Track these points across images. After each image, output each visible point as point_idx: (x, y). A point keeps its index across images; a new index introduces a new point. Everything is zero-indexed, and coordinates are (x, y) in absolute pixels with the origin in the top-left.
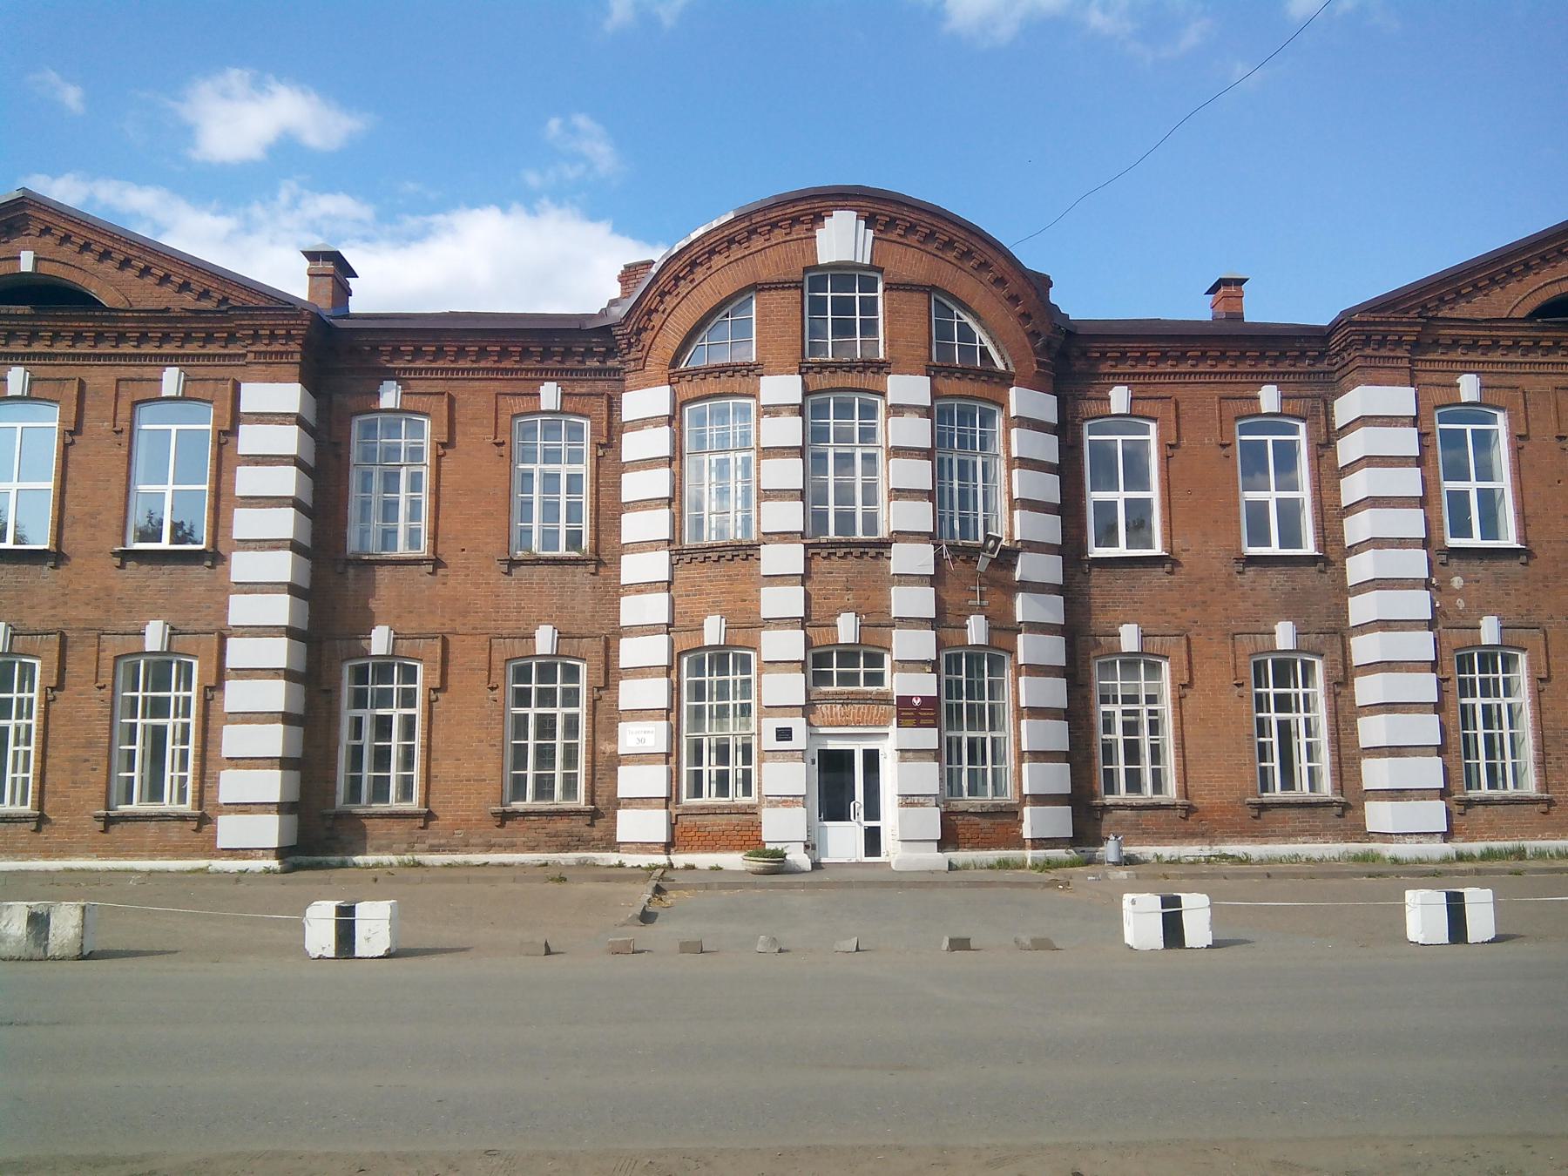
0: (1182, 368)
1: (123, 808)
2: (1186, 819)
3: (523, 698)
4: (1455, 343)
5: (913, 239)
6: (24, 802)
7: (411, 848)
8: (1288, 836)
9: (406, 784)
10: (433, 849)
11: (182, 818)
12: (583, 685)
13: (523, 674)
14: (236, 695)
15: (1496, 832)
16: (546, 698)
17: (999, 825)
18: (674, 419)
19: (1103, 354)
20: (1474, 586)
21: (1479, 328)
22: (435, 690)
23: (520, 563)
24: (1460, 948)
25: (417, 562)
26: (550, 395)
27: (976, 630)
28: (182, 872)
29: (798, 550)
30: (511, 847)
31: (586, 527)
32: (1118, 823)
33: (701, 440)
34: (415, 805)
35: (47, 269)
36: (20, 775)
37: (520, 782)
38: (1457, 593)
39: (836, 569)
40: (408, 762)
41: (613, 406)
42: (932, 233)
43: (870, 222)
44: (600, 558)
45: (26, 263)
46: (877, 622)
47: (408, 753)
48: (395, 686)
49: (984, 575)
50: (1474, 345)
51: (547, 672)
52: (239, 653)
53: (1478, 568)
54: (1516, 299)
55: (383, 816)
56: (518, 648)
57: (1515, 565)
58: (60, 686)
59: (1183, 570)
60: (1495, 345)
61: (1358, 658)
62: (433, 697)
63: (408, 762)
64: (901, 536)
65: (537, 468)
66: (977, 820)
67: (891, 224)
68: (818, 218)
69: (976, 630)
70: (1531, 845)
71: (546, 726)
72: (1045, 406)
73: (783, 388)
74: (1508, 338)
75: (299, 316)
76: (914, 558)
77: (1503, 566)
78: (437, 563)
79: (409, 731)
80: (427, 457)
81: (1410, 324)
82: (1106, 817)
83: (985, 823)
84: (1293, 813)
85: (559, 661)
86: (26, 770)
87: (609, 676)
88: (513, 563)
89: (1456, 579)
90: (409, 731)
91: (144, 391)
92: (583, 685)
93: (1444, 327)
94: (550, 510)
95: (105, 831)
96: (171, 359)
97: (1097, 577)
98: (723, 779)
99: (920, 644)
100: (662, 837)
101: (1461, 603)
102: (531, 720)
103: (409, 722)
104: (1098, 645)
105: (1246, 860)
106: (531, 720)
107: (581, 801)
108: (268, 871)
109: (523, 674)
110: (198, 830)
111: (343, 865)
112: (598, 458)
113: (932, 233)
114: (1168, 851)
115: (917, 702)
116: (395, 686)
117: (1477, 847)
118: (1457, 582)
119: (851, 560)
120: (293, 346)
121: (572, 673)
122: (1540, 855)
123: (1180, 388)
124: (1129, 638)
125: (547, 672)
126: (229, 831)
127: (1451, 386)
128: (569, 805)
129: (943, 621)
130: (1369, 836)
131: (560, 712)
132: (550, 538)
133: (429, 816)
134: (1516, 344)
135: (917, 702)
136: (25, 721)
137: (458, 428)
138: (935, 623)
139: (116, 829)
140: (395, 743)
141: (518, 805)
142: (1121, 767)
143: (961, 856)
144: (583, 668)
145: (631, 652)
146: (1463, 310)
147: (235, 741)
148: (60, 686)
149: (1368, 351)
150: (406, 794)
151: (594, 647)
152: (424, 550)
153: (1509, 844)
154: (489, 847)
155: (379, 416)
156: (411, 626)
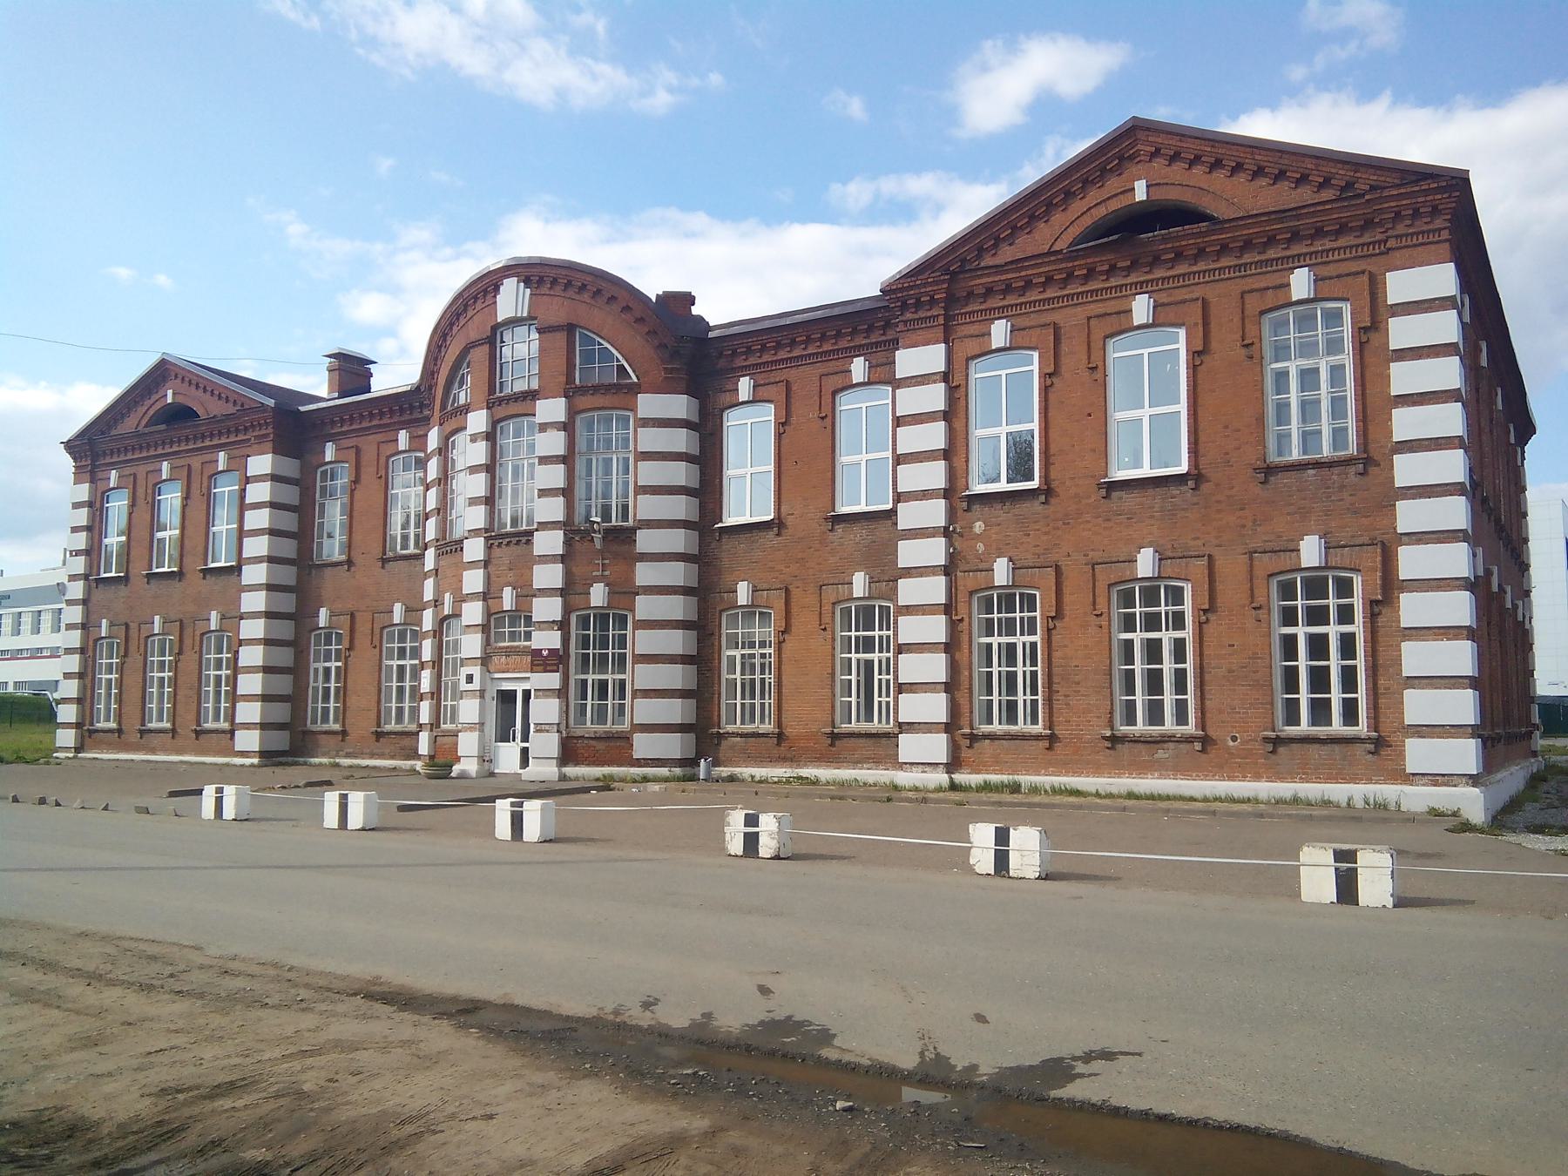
0: (796, 353)
1: (986, 728)
2: (780, 745)
3: (1289, 617)
4: (989, 292)
5: (558, 290)
6: (888, 722)
7: (337, 756)
8: (856, 763)
9: (1181, 707)
10: (348, 756)
11: (1038, 737)
12: (1188, 607)
13: (1288, 591)
14: (1413, 609)
15: (997, 764)
16: (1152, 622)
17: (616, 748)
18: (567, 427)
19: (734, 352)
20: (996, 529)
21: (1007, 272)
22: (1205, 611)
23: (389, 560)
24: (518, 844)
25: (1348, 462)
26: (1300, 283)
27: (598, 595)
28: (1280, 802)
29: (559, 535)
30: (382, 756)
31: (1351, 423)
32: (732, 747)
33: (590, 442)
34: (1191, 728)
35: (180, 399)
36: (884, 699)
37: (1292, 706)
38: (978, 537)
39: (503, 554)
40: (1180, 687)
41: (1376, 288)
42: (570, 282)
43: (527, 282)
44: (1372, 456)
45: (1140, 192)
46: (526, 593)
47: (1180, 676)
48: (1138, 610)
49: (601, 552)
50: (1008, 289)
51: (1151, 597)
52: (1412, 562)
53: (999, 512)
54: (1059, 231)
55: (326, 733)
56: (1285, 561)
57: (1036, 506)
58: (1059, 615)
59: (790, 531)
60: (1028, 284)
61: (1405, 571)
62: (1051, 625)
63: (1180, 687)
64: (544, 526)
65: (1293, 367)
66: (593, 743)
67: (541, 281)
68: (497, 289)
69: (598, 595)
70: (1026, 779)
71: (1318, 646)
72: (678, 405)
73: (552, 409)
74: (1039, 275)
75: (265, 411)
76: (549, 542)
77: (1026, 507)
78: (350, 562)
79: (1179, 655)
80: (1348, 345)
81: (935, 283)
82: (724, 743)
83: (600, 746)
84: (862, 741)
85: (1330, 574)
86: (888, 695)
87: (1389, 586)
88: (1270, 471)
89: (978, 524)
90: (1179, 655)
91: (209, 471)
92: (1188, 607)
93: (973, 278)
94: (1309, 409)
95: (832, 745)
96: (221, 447)
97: (728, 543)
98: (1012, 707)
99: (547, 609)
100: (943, 758)
101: (981, 547)
102: (995, 647)
103: (1179, 645)
104: (722, 599)
105: (816, 782)
106: (995, 647)
107: (1362, 728)
108: (252, 765)
109: (1288, 591)
110: (1203, 751)
111: (305, 764)
112: (1361, 343)
113: (570, 282)
114: (760, 772)
115: (545, 653)
116: (1138, 610)
117: (974, 779)
118: (979, 527)
119: (513, 547)
120: (270, 430)
121: (1176, 596)
122: (1035, 790)
123: (793, 371)
124: (743, 594)
125: (1316, 587)
126: (1419, 754)
127: (983, 335)
128: (1350, 731)
129: (570, 591)
130: (903, 766)
131: (1333, 631)
132: (1310, 438)
133: (344, 733)
134: (1049, 280)
135: (545, 653)
136: (885, 654)
137: (363, 470)
138: (563, 592)
139: (146, 736)
140: (1334, 663)
141: (1292, 730)
142: (1140, 698)
143: (570, 771)
144: (1358, 582)
145: (934, 590)
146: (1007, 254)
147: (1416, 658)
148: (1059, 615)
149: (909, 316)
150: (1181, 718)
151: (1373, 557)
152: (1352, 449)
153: (1005, 778)
154: (372, 756)
155: (1290, 312)
156: (339, 606)
